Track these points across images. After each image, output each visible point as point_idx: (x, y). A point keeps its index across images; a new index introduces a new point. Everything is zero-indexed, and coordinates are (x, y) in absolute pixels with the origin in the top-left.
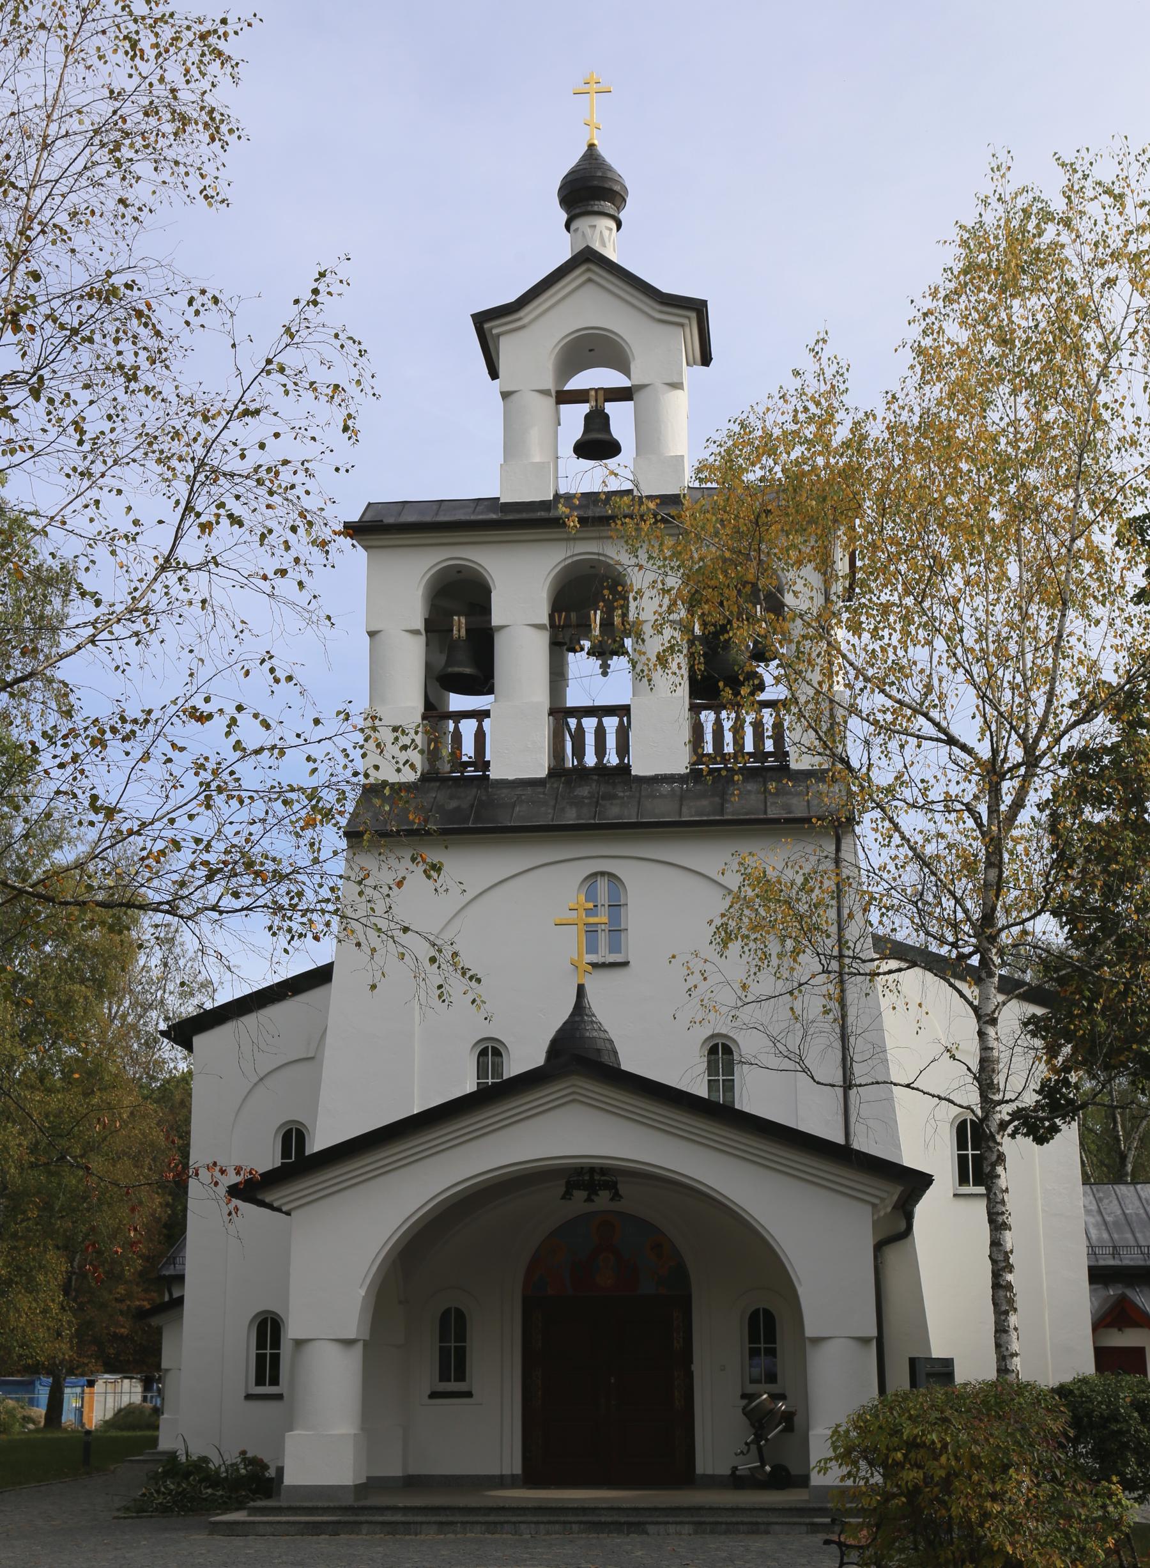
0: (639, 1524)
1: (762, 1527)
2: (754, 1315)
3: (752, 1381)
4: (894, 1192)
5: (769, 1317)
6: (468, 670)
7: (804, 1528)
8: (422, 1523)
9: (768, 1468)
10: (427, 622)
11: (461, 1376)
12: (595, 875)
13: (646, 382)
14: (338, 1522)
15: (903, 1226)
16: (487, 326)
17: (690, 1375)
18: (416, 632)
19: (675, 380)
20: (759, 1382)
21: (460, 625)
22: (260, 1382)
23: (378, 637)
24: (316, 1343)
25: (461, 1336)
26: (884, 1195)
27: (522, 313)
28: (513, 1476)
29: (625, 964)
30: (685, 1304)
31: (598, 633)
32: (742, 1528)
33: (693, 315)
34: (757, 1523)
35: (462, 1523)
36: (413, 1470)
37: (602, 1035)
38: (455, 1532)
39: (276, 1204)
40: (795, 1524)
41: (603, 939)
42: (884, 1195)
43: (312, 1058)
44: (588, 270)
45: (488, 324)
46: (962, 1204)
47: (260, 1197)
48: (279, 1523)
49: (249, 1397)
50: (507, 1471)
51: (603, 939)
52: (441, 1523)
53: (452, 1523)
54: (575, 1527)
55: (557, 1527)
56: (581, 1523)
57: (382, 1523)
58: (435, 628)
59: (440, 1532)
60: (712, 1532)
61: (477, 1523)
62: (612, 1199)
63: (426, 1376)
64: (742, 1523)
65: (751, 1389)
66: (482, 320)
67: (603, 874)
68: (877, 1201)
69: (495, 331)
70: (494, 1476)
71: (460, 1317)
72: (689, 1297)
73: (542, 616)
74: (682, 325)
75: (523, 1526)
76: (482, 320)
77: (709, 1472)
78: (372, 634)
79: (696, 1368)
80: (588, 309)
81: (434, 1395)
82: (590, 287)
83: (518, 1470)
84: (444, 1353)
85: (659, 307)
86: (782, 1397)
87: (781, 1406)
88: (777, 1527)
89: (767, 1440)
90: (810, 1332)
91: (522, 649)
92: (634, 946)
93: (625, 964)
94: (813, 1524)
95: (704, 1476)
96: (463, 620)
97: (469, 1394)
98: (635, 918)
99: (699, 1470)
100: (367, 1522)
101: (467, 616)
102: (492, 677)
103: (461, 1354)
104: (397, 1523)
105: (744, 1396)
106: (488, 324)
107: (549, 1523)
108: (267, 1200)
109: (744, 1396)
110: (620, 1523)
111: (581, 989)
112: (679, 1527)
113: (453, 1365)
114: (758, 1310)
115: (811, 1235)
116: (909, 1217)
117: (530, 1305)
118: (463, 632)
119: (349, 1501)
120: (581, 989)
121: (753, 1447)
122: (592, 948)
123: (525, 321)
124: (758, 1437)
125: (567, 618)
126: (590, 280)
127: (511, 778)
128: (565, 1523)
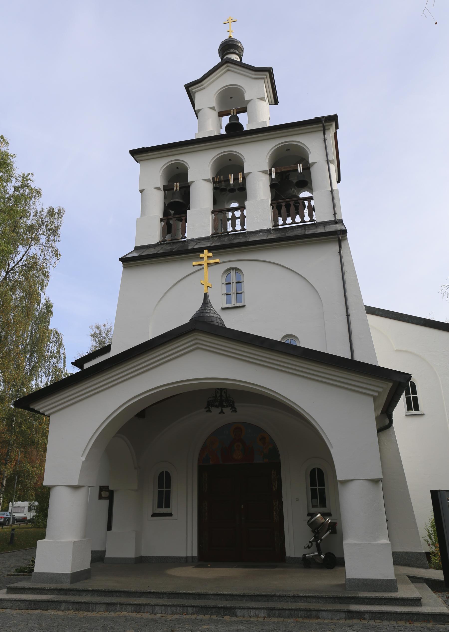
0: (231, 608)
1: (314, 613)
2: (313, 472)
3: (313, 506)
4: (385, 387)
5: (320, 472)
6: (179, 200)
7: (343, 615)
8: (96, 603)
9: (322, 556)
10: (164, 186)
11: (168, 505)
12: (229, 270)
13: (250, 99)
14: (48, 601)
15: (387, 422)
16: (190, 89)
17: (281, 503)
18: (158, 188)
19: (262, 97)
20: (317, 506)
21: (177, 186)
23: (143, 192)
24: (57, 488)
25: (168, 485)
26: (381, 390)
27: (203, 83)
28: (193, 557)
29: (244, 306)
30: (277, 467)
31: (232, 182)
32: (300, 613)
33: (267, 73)
34: (310, 610)
35: (121, 604)
36: (144, 553)
37: (215, 315)
38: (116, 611)
39: (41, 411)
40: (337, 611)
41: (234, 297)
42: (381, 390)
44: (228, 66)
45: (191, 88)
46: (410, 419)
47: (32, 407)
48: (15, 600)
50: (189, 555)
51: (234, 297)
53: (114, 604)
54: (190, 609)
55: (178, 609)
56: (193, 606)
57: (74, 603)
58: (167, 189)
59: (107, 611)
61: (129, 604)
63: (150, 504)
64: (300, 610)
65: (313, 510)
66: (188, 87)
67: (233, 269)
68: (376, 394)
70: (182, 558)
71: (168, 476)
72: (279, 463)
73: (209, 176)
74: (264, 79)
75: (157, 608)
76: (188, 87)
77: (293, 556)
78: (141, 191)
79: (284, 499)
80: (229, 79)
81: (154, 515)
82: (229, 72)
83: (195, 554)
84: (160, 493)
85: (254, 73)
86: (329, 515)
87: (329, 520)
88: (324, 614)
89: (321, 540)
90: (340, 477)
91: (202, 197)
92: (247, 299)
93: (244, 306)
94: (350, 612)
96: (178, 184)
97: (170, 515)
98: (248, 287)
99: (288, 555)
100: (64, 602)
101: (179, 183)
102: (189, 203)
103: (168, 494)
105: (309, 514)
106: (191, 88)
107: (174, 606)
108: (36, 409)
109: (309, 514)
110: (219, 608)
111: (206, 295)
112: (257, 612)
113: (164, 500)
115: (336, 417)
116: (390, 417)
117: (202, 469)
118: (178, 188)
119: (67, 586)
120: (206, 295)
121: (314, 543)
122: (228, 302)
123: (205, 85)
124: (317, 538)
125: (220, 178)
126: (228, 70)
127: (195, 238)
128: (183, 606)
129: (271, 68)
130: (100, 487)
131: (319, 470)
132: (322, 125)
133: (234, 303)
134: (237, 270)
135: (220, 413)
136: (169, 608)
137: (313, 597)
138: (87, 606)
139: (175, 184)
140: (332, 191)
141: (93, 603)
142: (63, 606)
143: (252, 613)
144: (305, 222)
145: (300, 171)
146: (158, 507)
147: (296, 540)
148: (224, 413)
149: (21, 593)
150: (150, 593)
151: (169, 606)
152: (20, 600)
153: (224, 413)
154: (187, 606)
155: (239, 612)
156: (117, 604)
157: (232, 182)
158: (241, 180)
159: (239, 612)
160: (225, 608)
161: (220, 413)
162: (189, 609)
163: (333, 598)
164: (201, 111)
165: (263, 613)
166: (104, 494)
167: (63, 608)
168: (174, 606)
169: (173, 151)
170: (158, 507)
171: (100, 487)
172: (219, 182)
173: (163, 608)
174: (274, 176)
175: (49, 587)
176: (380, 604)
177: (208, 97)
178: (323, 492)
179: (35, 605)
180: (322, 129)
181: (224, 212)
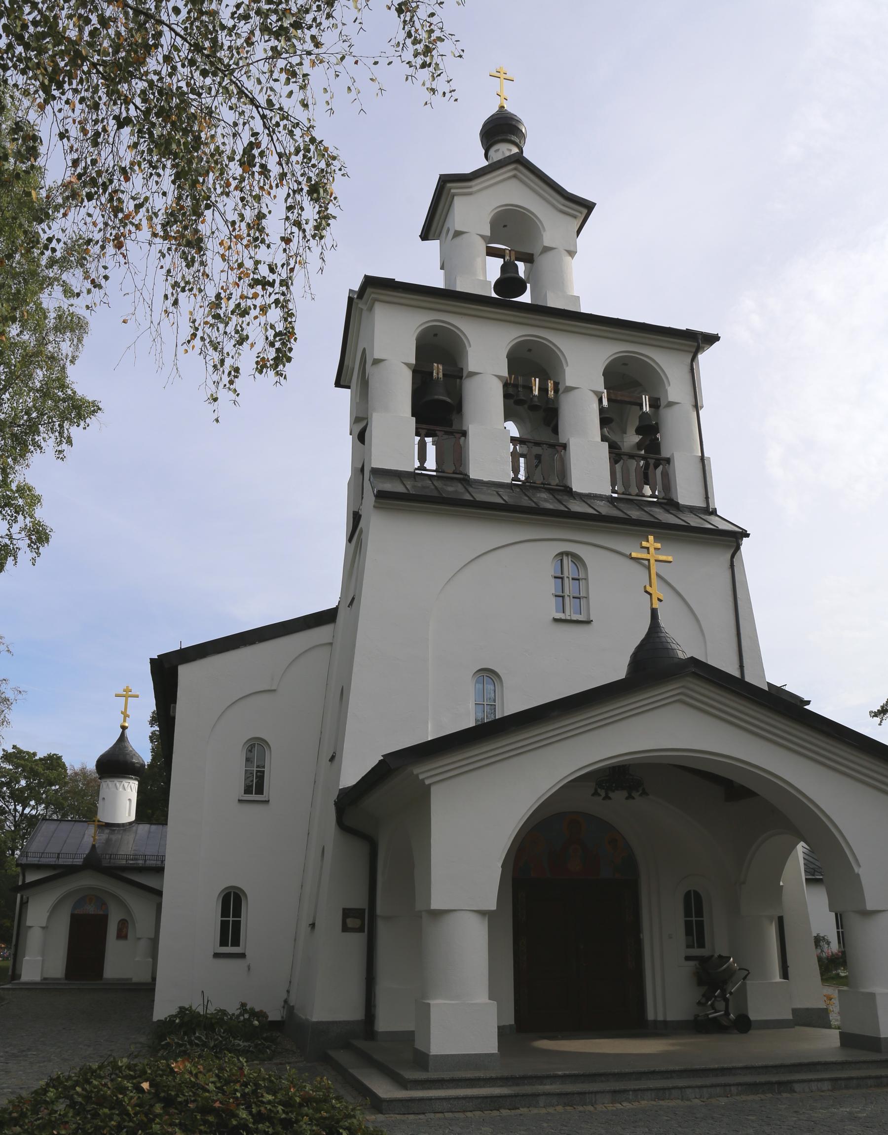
2: (688, 895)
5: (697, 895)
8: (596, 1093)
13: (554, 246)
16: (449, 185)
17: (639, 943)
22: (223, 942)
34: (881, 1077)
35: (635, 1091)
43: (274, 690)
44: (515, 169)
48: (457, 1098)
49: (217, 955)
52: (615, 1092)
53: (536, 1095)
55: (718, 1090)
57: (560, 1095)
59: (613, 1102)
60: (847, 1087)
62: (627, 798)
64: (870, 1077)
67: (567, 554)
69: (452, 191)
75: (689, 1091)
79: (646, 936)
82: (514, 182)
93: (588, 622)
95: (655, 1022)
96: (441, 367)
99: (651, 1016)
100: (689, 1087)
101: (443, 365)
104: (573, 1094)
107: (712, 1086)
111: (654, 613)
114: (689, 892)
118: (441, 375)
120: (654, 613)
126: (515, 176)
128: (725, 1085)
129: (441, 175)
130: (344, 910)
131: (696, 892)
132: (696, 344)
133: (569, 614)
134: (576, 558)
135: (593, 795)
136: (705, 1090)
137: (864, 1062)
138: (531, 1099)
139: (435, 365)
140: (702, 458)
141: (592, 1093)
142: (542, 1101)
143: (814, 1086)
144: (425, 469)
145: (646, 408)
146: (221, 945)
147: (668, 988)
148: (610, 798)
149: (435, 1089)
150: (653, 1072)
151: (706, 1086)
152: (465, 1098)
153: (610, 798)
154: (730, 1085)
155: (797, 1087)
156: (629, 1091)
157: (536, 393)
158: (551, 393)
159: (797, 1087)
160: (780, 1083)
161: (593, 795)
162: (732, 1088)
163: (497, 1079)
164: (464, 236)
165: (826, 1086)
166: (350, 922)
167: (541, 1104)
168: (712, 1086)
169: (402, 297)
170: (221, 945)
171: (344, 910)
172: (516, 386)
173: (697, 1090)
174: (605, 403)
175: (488, 1076)
176: (457, 1087)
177: (472, 214)
178: (700, 925)
179: (494, 1102)
180: (694, 350)
181: (457, 435)
